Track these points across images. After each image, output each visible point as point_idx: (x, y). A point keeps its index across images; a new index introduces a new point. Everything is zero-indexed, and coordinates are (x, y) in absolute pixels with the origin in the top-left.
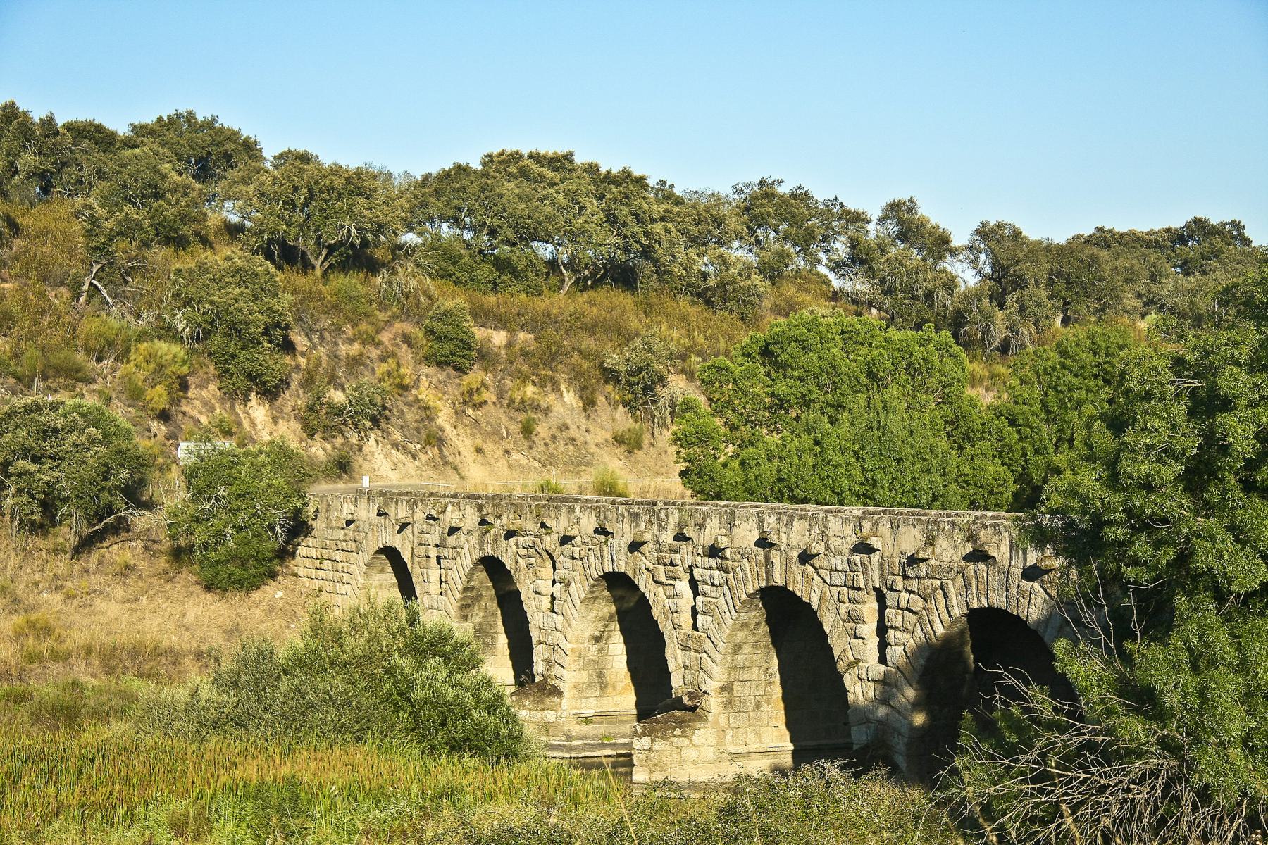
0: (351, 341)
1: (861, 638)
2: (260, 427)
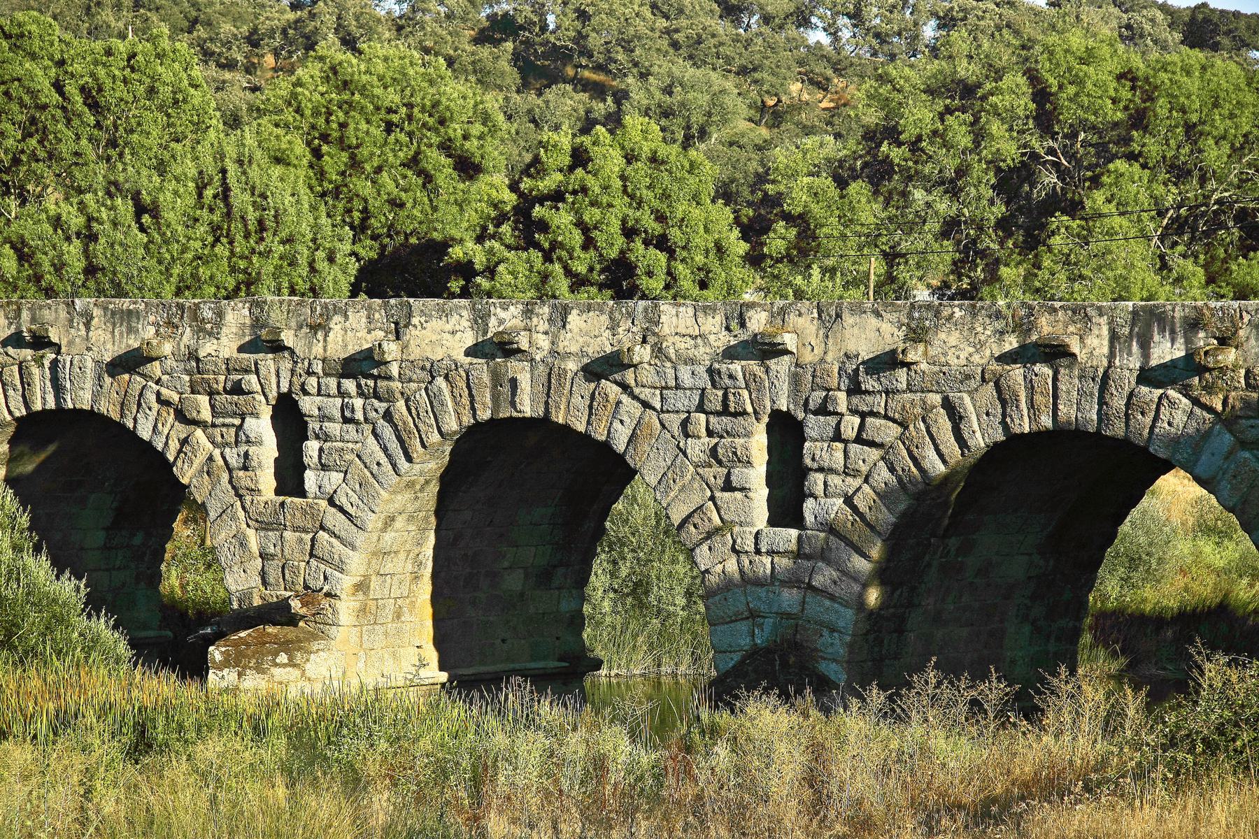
1: (742, 489)
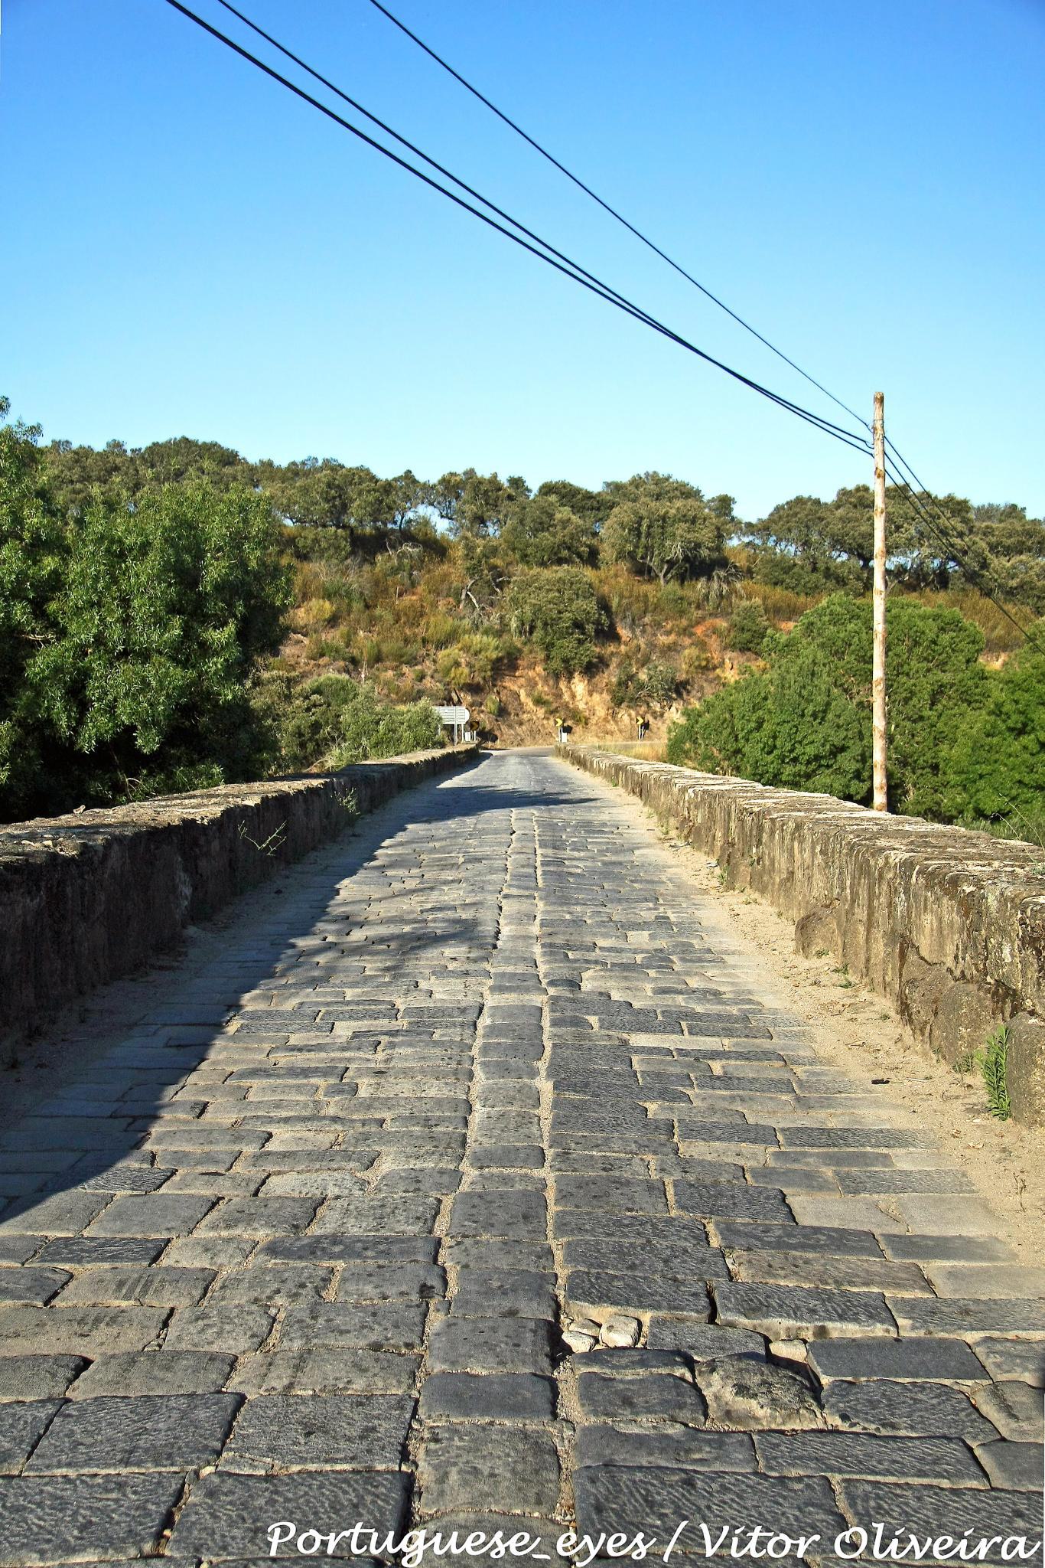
0: (668, 633)
2: (578, 698)
